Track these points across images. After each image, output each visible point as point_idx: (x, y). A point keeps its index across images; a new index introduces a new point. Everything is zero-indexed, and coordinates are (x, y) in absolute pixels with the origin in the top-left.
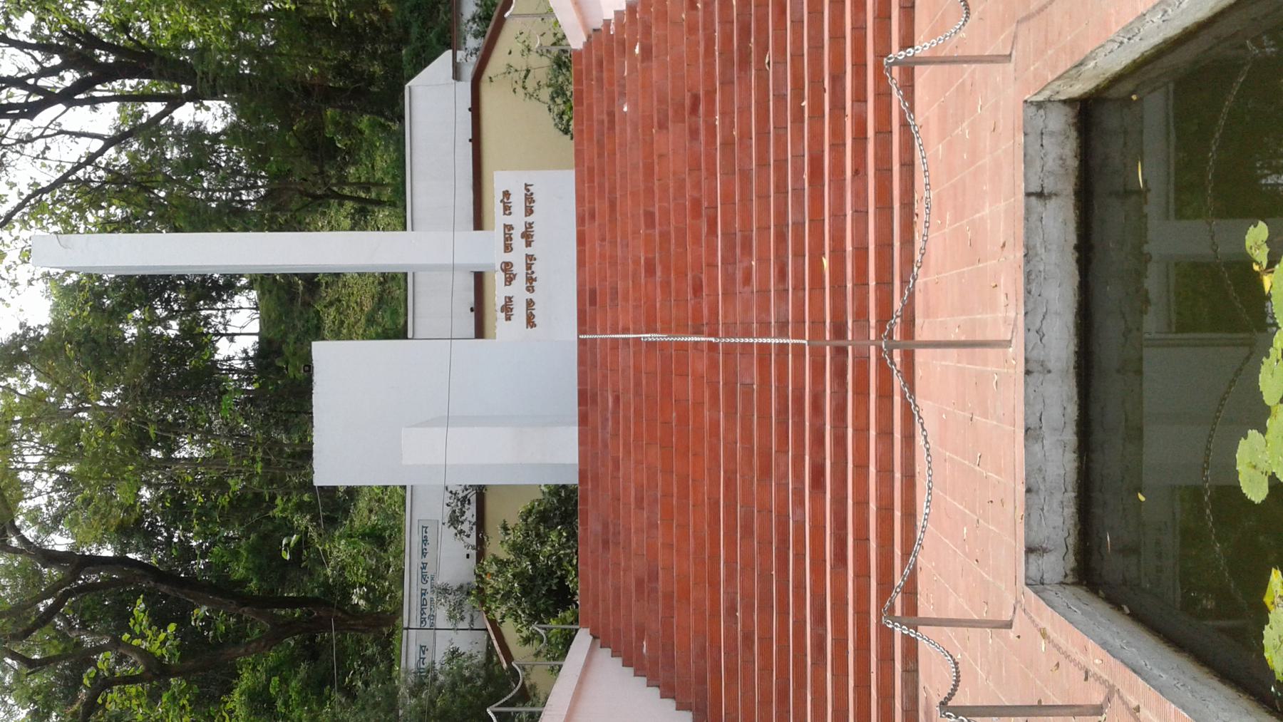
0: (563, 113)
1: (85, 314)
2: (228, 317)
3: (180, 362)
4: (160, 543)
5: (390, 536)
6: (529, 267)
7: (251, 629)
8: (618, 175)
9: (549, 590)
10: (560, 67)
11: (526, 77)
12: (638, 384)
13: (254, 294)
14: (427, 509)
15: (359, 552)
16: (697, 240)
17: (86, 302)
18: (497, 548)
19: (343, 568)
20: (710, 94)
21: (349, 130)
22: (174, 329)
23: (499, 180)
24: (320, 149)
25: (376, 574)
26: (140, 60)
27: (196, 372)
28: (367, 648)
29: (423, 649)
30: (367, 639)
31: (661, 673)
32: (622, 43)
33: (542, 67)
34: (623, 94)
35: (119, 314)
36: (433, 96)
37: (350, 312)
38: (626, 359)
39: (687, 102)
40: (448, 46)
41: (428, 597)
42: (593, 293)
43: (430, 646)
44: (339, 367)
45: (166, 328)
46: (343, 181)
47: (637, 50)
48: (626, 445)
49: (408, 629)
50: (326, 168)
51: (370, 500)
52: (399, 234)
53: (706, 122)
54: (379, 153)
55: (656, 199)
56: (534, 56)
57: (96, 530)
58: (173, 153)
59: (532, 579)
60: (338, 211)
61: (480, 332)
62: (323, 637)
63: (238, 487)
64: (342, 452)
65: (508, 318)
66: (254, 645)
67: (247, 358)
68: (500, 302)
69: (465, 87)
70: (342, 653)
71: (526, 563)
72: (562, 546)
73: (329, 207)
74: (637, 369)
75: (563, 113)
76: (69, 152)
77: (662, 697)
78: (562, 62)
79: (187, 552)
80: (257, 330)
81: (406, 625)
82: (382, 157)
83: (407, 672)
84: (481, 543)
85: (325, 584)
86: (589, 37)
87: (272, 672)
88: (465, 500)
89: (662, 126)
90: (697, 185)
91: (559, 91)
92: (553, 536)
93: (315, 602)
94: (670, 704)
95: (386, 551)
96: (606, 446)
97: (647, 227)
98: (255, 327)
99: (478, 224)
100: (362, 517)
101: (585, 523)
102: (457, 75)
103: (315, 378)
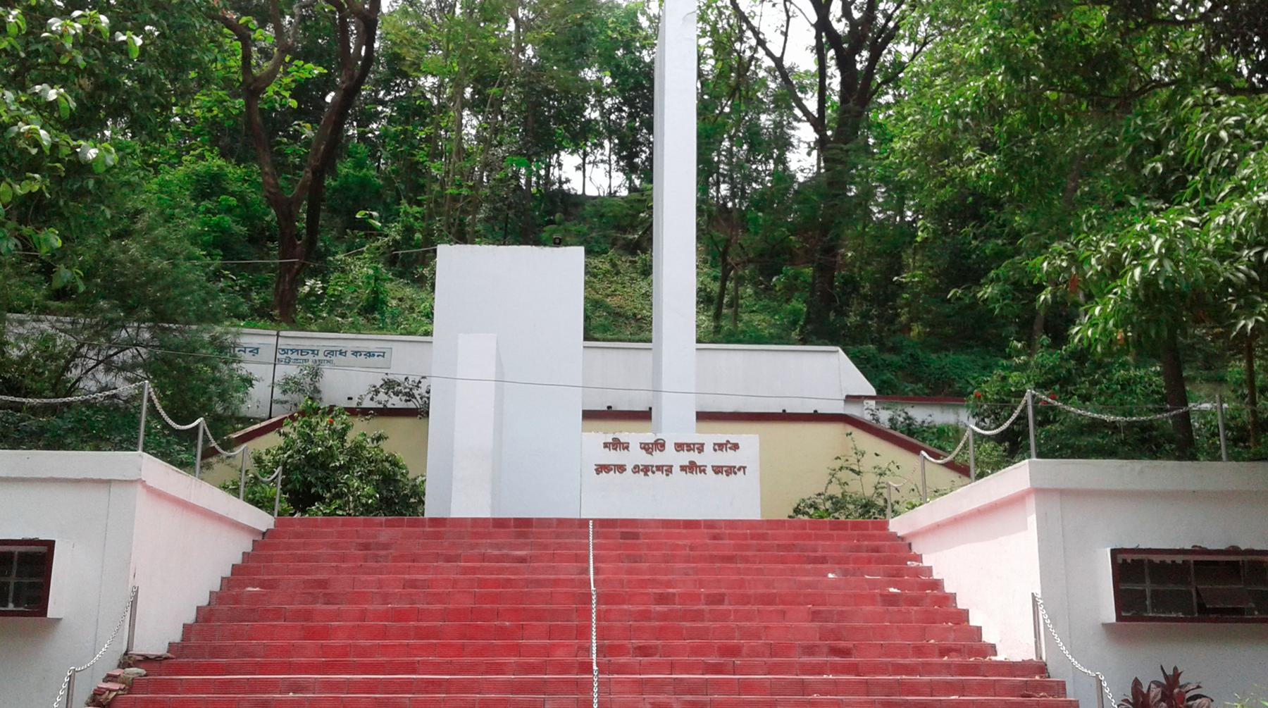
0: (816, 508)
1: (610, 33)
2: (601, 165)
3: (559, 118)
4: (377, 93)
5: (374, 319)
6: (659, 468)
7: (286, 179)
8: (761, 566)
9: (310, 485)
10: (865, 506)
11: (852, 470)
12: (539, 583)
13: (624, 193)
14: (402, 357)
15: (360, 287)
16: (695, 651)
17: (621, 34)
18: (359, 429)
19: (343, 271)
20: (853, 669)
21: (790, 290)
22: (592, 114)
23: (749, 438)
24: (770, 260)
25: (336, 303)
26: (858, 92)
27: (552, 133)
28: (258, 293)
29: (255, 351)
30: (269, 294)
31: (225, 607)
33: (864, 487)
34: (846, 573)
35: (609, 64)
36: (828, 376)
37: (606, 284)
38: (567, 571)
39: (842, 644)
40: (878, 391)
41: (310, 357)
43: (257, 357)
44: (561, 270)
45: (593, 106)
46: (740, 281)
47: (892, 590)
48: (473, 571)
49: (278, 335)
50: (752, 266)
51: (412, 299)
52: (692, 334)
53: (825, 664)
54: (768, 318)
55: (736, 607)
56: (875, 479)
57: (396, 35)
58: (765, 119)
59: (324, 466)
60: (709, 275)
61: (589, 415)
62: (271, 249)
63: (434, 172)
64: (466, 272)
65: (606, 445)
66: (271, 181)
68: (623, 437)
69: (839, 408)
70: (256, 269)
71: (342, 460)
73: (712, 266)
74: (556, 583)
75: (816, 508)
76: (768, 20)
77: (199, 609)
79: (366, 118)
80: (588, 193)
81: (282, 333)
83: (238, 334)
84: (365, 412)
85: (328, 252)
86: (902, 538)
87: (241, 197)
88: (410, 396)
89: (815, 615)
90: (755, 653)
91: (838, 504)
92: (368, 489)
93: (311, 241)
94: (190, 617)
95: (359, 314)
96: (472, 547)
97: (708, 596)
98: (592, 191)
99: (702, 416)
100: (396, 291)
101: (389, 524)
102: (850, 399)
103: (547, 249)
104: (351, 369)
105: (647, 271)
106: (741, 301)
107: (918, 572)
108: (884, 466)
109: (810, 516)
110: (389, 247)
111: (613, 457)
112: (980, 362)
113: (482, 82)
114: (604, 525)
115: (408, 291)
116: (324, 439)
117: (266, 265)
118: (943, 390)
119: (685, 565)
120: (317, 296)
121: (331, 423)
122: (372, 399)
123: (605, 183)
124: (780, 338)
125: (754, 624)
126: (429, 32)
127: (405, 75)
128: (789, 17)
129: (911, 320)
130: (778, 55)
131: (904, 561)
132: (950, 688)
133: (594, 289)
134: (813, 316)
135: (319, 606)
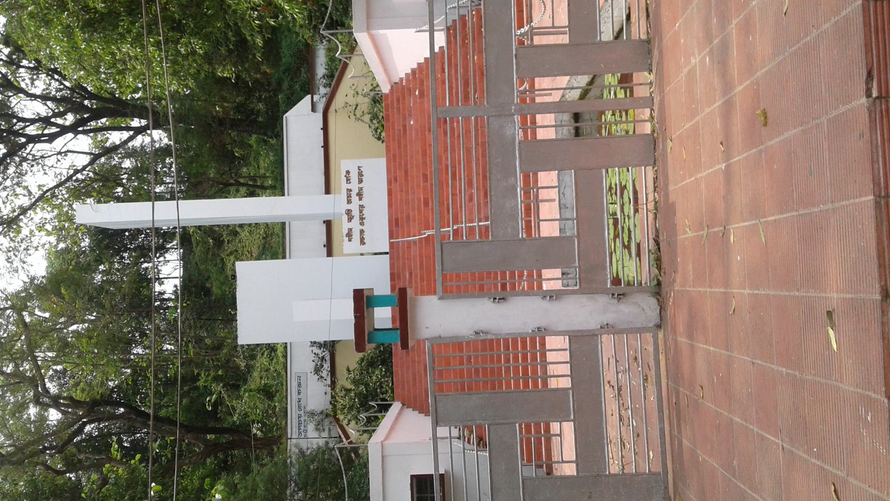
6: (361, 212)
10: (375, 102)
12: (421, 264)
14: (302, 362)
18: (344, 381)
23: (343, 165)
32: (409, 89)
33: (365, 103)
34: (410, 115)
36: (300, 123)
38: (415, 251)
41: (302, 419)
42: (397, 220)
47: (682, 41)
51: (261, 371)
65: (350, 240)
67: (175, 292)
69: (319, 116)
71: (362, 388)
72: (383, 377)
74: (421, 256)
76: (64, 167)
78: (377, 100)
81: (289, 436)
82: (264, 161)
86: (392, 87)
88: (323, 359)
91: (375, 116)
98: (178, 273)
102: (313, 109)
104: (309, 392)
107: (408, 80)
110: (228, 390)
111: (356, 236)
112: (286, 33)
115: (255, 374)
116: (351, 399)
118: (306, 56)
120: (262, 427)
123: (171, 265)
126: (80, 382)
131: (403, 87)
134: (262, 131)
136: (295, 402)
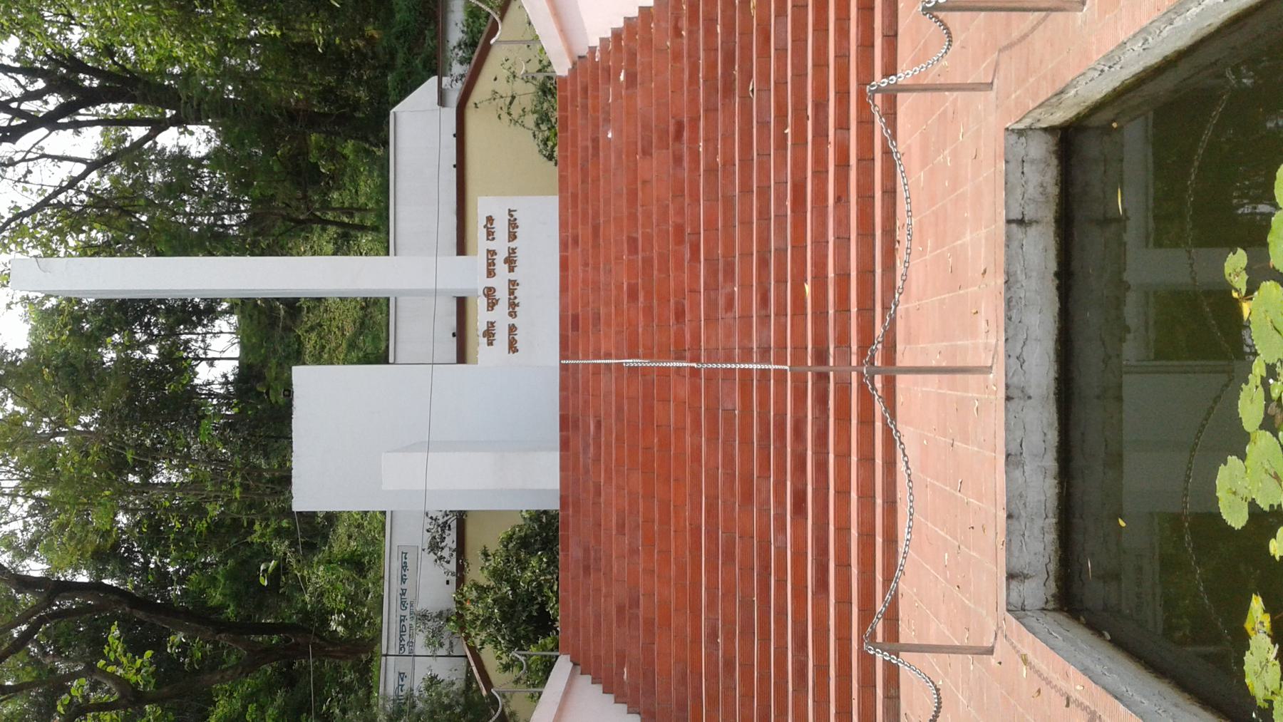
0: (548, 139)
1: (64, 338)
3: (159, 387)
6: (511, 292)
9: (530, 617)
10: (544, 93)
11: (511, 103)
12: (619, 409)
14: (408, 536)
15: (338, 578)
16: (679, 266)
17: (65, 326)
18: (478, 574)
20: (694, 121)
21: (333, 155)
22: (153, 353)
23: (482, 206)
24: (303, 174)
26: (123, 84)
29: (402, 676)
30: (346, 665)
33: (527, 93)
34: (607, 120)
36: (419, 122)
37: (332, 337)
38: (608, 384)
39: (672, 129)
40: (434, 72)
41: (407, 623)
42: (575, 318)
43: (408, 673)
44: (317, 390)
46: (326, 206)
47: (622, 77)
48: (608, 470)
50: (310, 193)
51: (350, 525)
52: (383, 258)
53: (690, 149)
58: (156, 178)
59: (512, 605)
60: (320, 235)
61: (462, 358)
62: (300, 664)
64: (322, 476)
65: (490, 344)
68: (482, 327)
69: (450, 113)
71: (506, 589)
72: (543, 572)
74: (619, 396)
75: (548, 139)
76: (50, 176)
78: (548, 88)
79: (163, 578)
81: (384, 652)
83: (385, 697)
84: (461, 569)
85: (303, 610)
86: (574, 64)
87: (249, 698)
88: (445, 526)
89: (646, 152)
90: (680, 212)
91: (544, 118)
92: (534, 562)
93: (292, 628)
95: (365, 577)
97: (630, 253)
98: (235, 352)
99: (461, 249)
100: (341, 543)
101: (566, 549)
102: (442, 101)
105: (318, 301)
106: (346, 204)
108: (506, 73)
109: (555, 145)
111: (502, 336)
113: (121, 466)
114: (566, 348)
115: (341, 530)
117: (316, 668)
119: (602, 272)
121: (472, 601)
122: (448, 562)
123: (225, 339)
124: (382, 167)
125: (655, 210)
127: (116, 546)
128: (43, 156)
129: (362, 37)
130: (82, 167)
131: (595, 65)
132: (710, 32)
133: (337, 348)
135: (641, 613)
136: (395, 594)
